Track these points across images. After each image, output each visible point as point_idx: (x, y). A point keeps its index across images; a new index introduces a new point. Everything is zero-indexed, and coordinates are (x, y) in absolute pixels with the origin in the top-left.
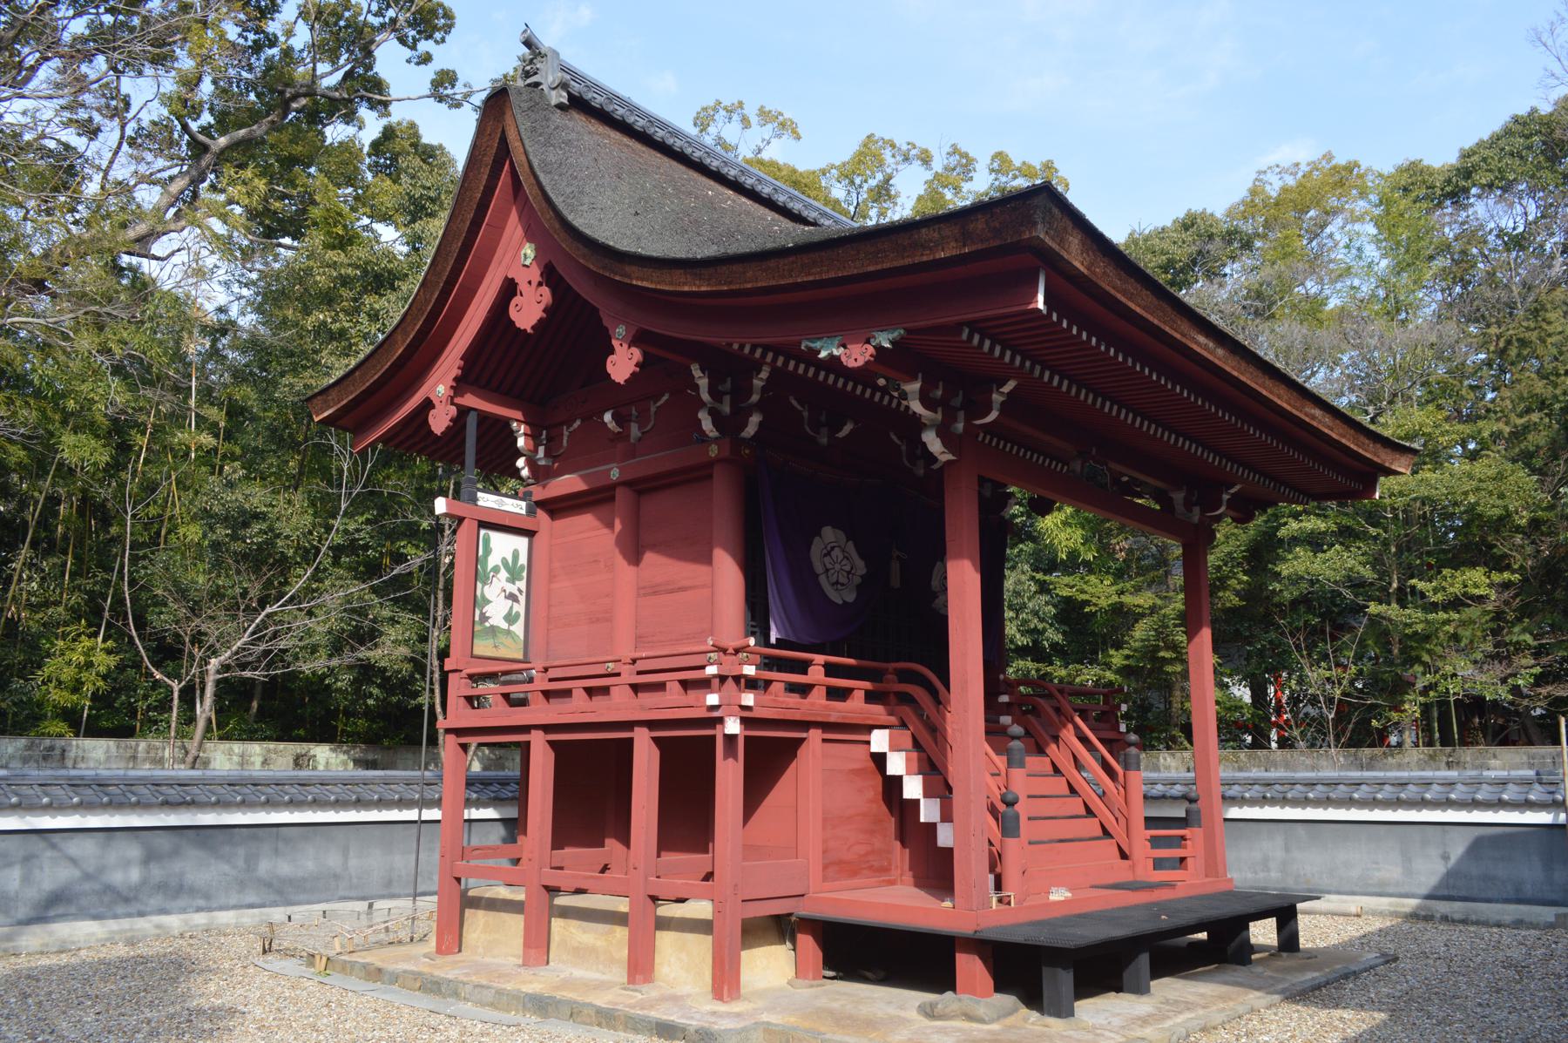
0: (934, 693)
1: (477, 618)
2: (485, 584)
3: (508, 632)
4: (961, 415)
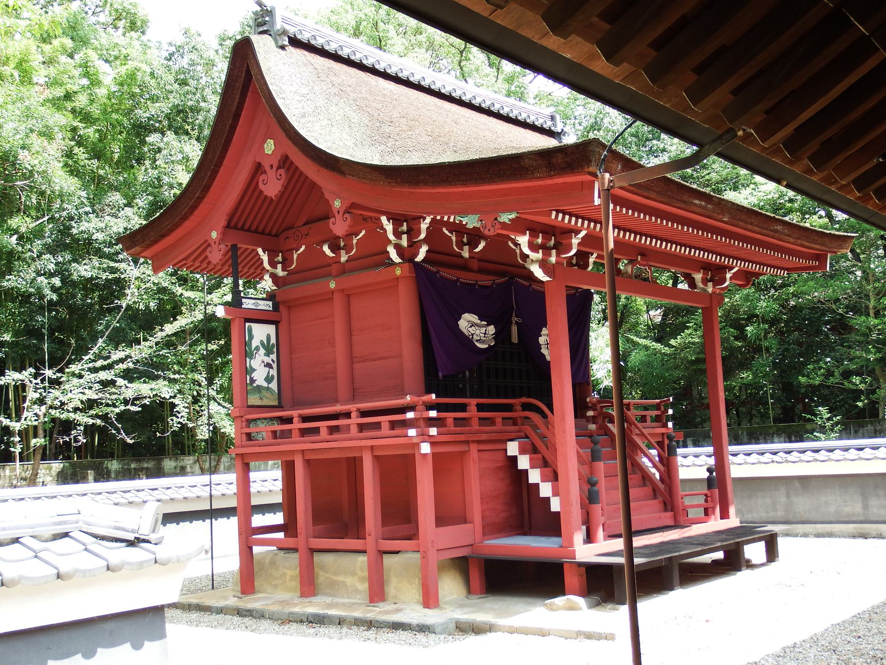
0: (545, 416)
1: (248, 382)
2: (251, 359)
3: (268, 388)
4: (554, 252)
